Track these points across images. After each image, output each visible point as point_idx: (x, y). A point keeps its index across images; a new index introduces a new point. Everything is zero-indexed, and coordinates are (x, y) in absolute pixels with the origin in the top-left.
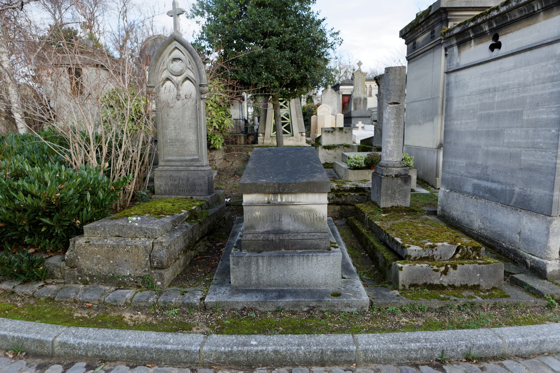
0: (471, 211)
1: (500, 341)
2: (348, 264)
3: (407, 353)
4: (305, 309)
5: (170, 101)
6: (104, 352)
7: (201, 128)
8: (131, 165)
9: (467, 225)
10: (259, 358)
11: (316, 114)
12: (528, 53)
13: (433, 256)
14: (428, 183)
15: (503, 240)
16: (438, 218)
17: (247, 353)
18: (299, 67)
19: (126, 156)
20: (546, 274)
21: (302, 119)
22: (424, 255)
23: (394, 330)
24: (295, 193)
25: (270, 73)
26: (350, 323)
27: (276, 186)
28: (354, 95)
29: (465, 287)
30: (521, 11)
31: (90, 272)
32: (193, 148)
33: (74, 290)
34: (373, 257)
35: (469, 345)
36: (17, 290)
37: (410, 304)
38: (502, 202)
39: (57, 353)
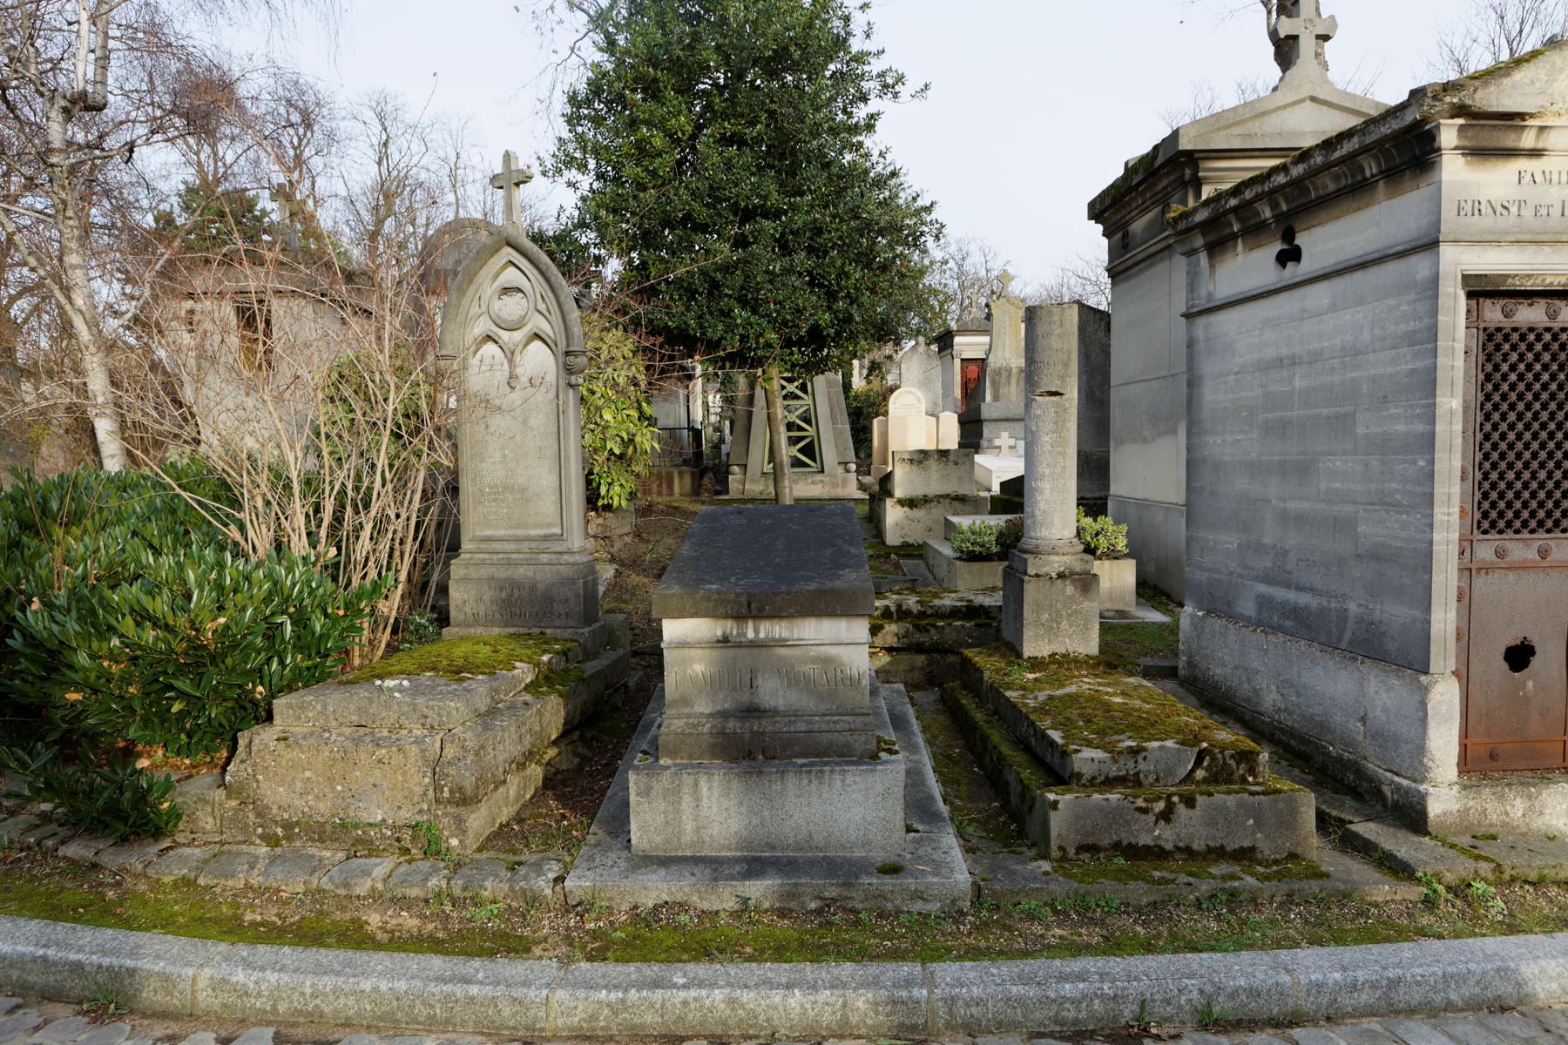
0: (1255, 664)
1: (1287, 978)
2: (932, 798)
3: (1055, 1007)
4: (813, 905)
5: (493, 392)
6: (318, 1001)
7: (567, 458)
8: (392, 549)
9: (1248, 700)
10: (690, 1016)
11: (886, 414)
12: (1359, 276)
13: (1137, 774)
14: (1168, 596)
15: (1329, 737)
16: (1181, 685)
17: (663, 1005)
18: (831, 296)
19: (379, 528)
20: (1426, 822)
21: (848, 427)
22: (1114, 771)
23: (1025, 954)
24: (790, 616)
25: (754, 311)
26: (922, 938)
27: (743, 599)
28: (991, 359)
29: (1218, 853)
30: (1337, 178)
31: (286, 816)
32: (547, 507)
33: (244, 859)
34: (994, 779)
35: (1209, 988)
36: (106, 859)
37: (1076, 893)
38: (1323, 639)
39: (203, 1005)
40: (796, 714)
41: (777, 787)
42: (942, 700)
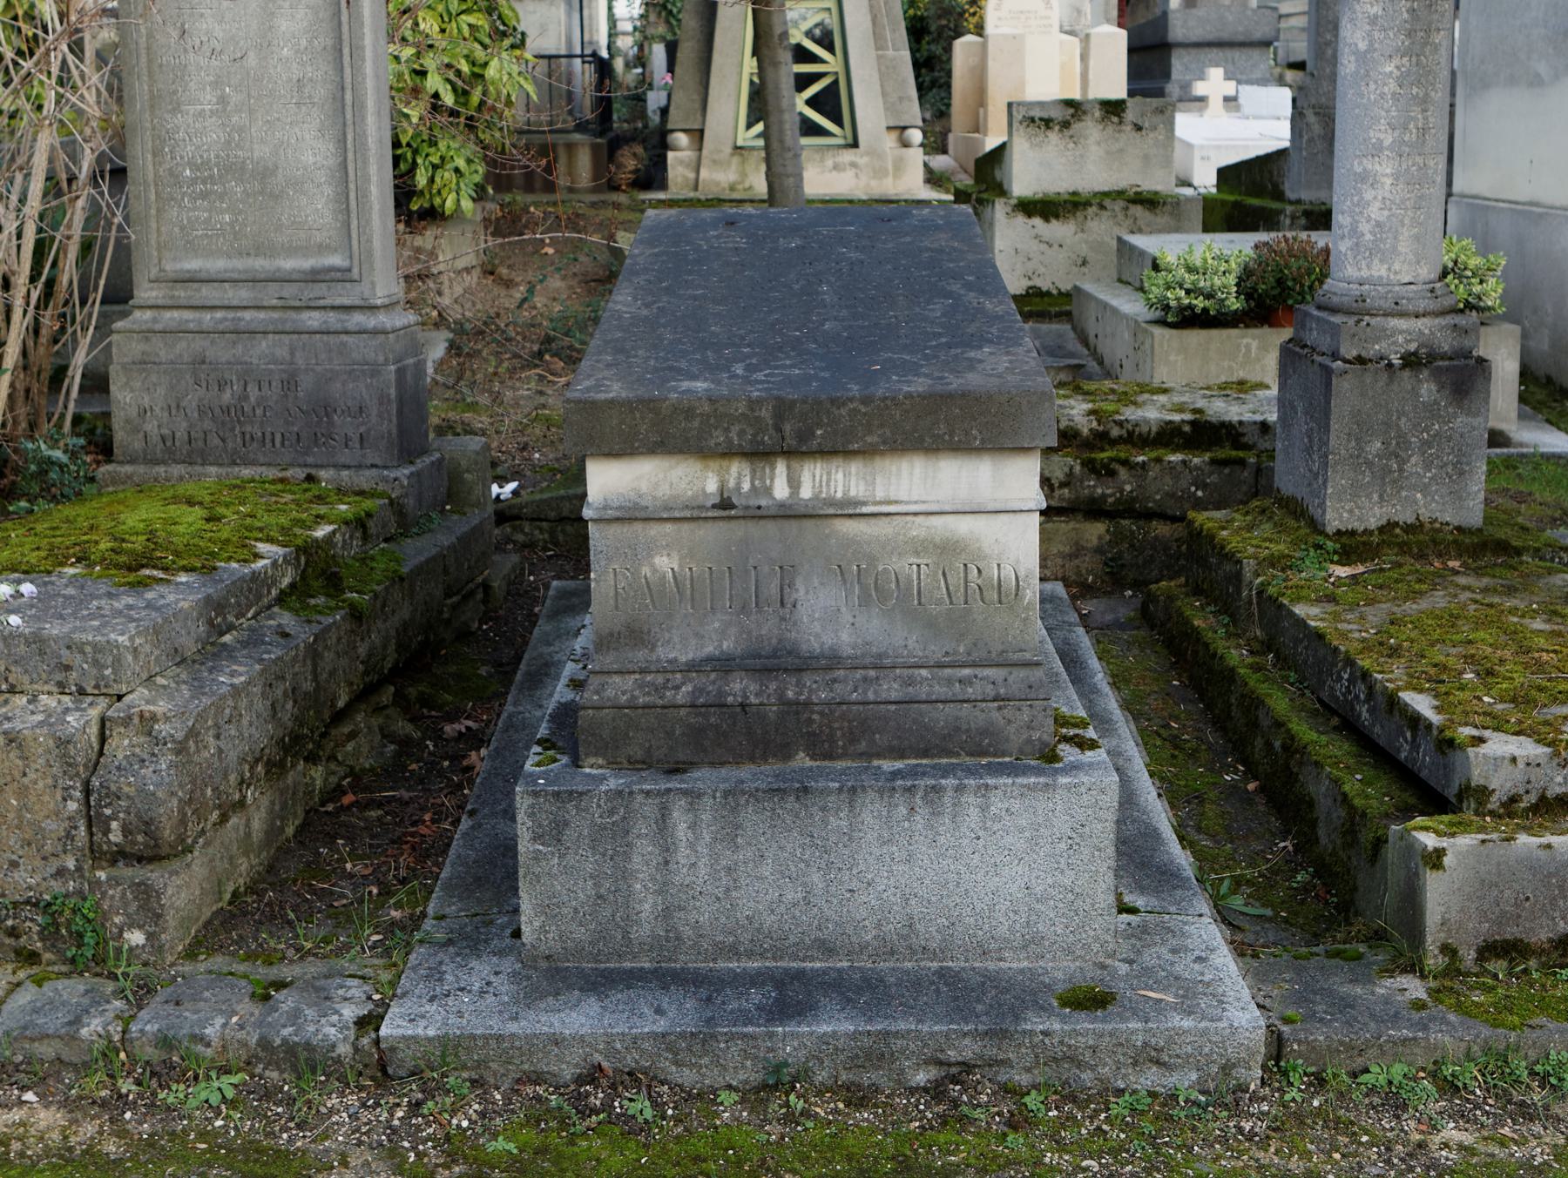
2: (1154, 835)
4: (921, 1078)
11: (980, 30)
21: (906, 55)
24: (868, 452)
27: (765, 413)
32: (316, 208)
34: (1283, 793)
37: (1487, 1050)
40: (881, 664)
41: (839, 822)
42: (1146, 615)
